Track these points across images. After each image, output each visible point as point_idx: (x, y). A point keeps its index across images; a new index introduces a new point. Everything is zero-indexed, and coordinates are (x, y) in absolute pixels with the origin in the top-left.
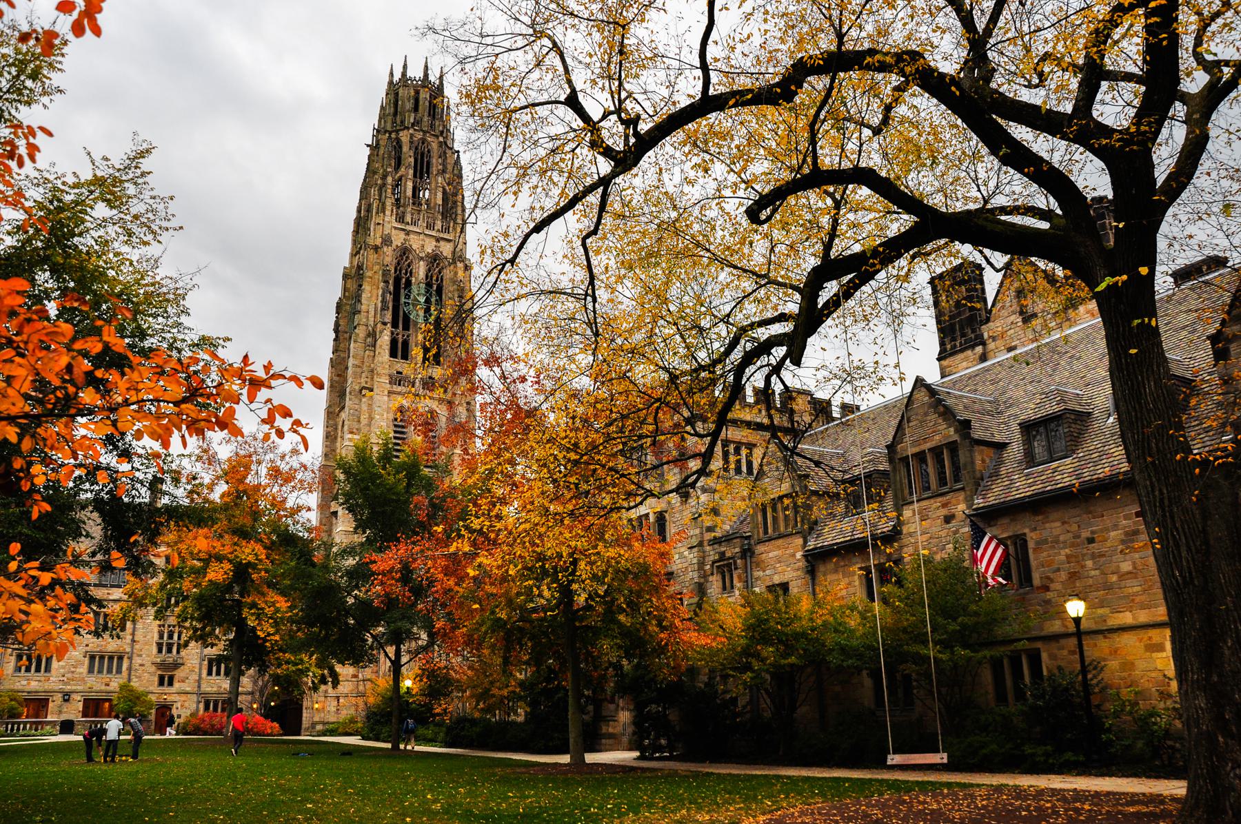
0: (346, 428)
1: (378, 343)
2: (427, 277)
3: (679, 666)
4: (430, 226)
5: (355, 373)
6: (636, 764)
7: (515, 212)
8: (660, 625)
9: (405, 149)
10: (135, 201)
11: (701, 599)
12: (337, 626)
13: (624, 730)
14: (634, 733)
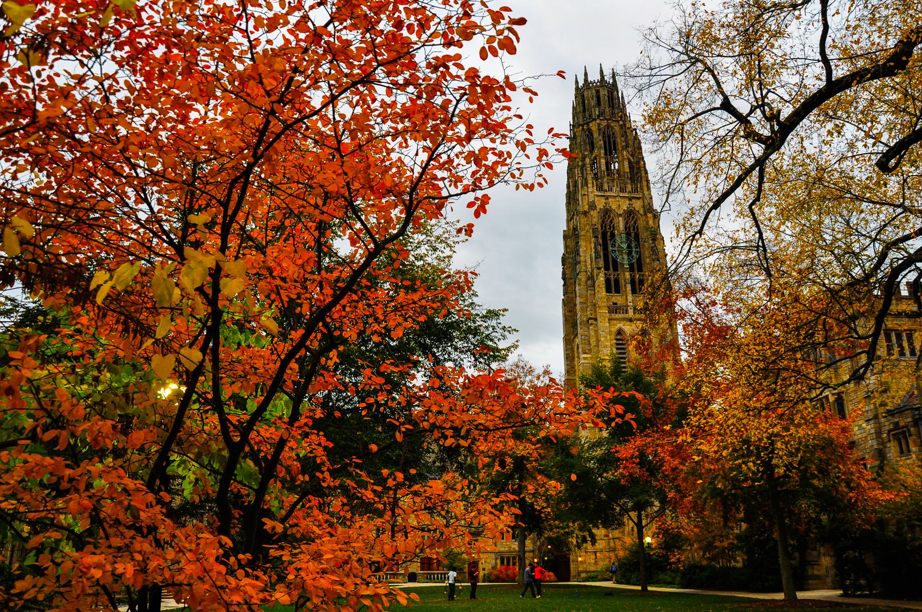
0: (580, 350)
1: (597, 283)
2: (626, 228)
3: (870, 518)
4: (622, 190)
5: (582, 308)
6: (840, 600)
7: (696, 195)
8: (848, 486)
9: (596, 135)
10: (436, 227)
11: (882, 462)
12: (594, 502)
13: (827, 572)
14: (836, 575)
